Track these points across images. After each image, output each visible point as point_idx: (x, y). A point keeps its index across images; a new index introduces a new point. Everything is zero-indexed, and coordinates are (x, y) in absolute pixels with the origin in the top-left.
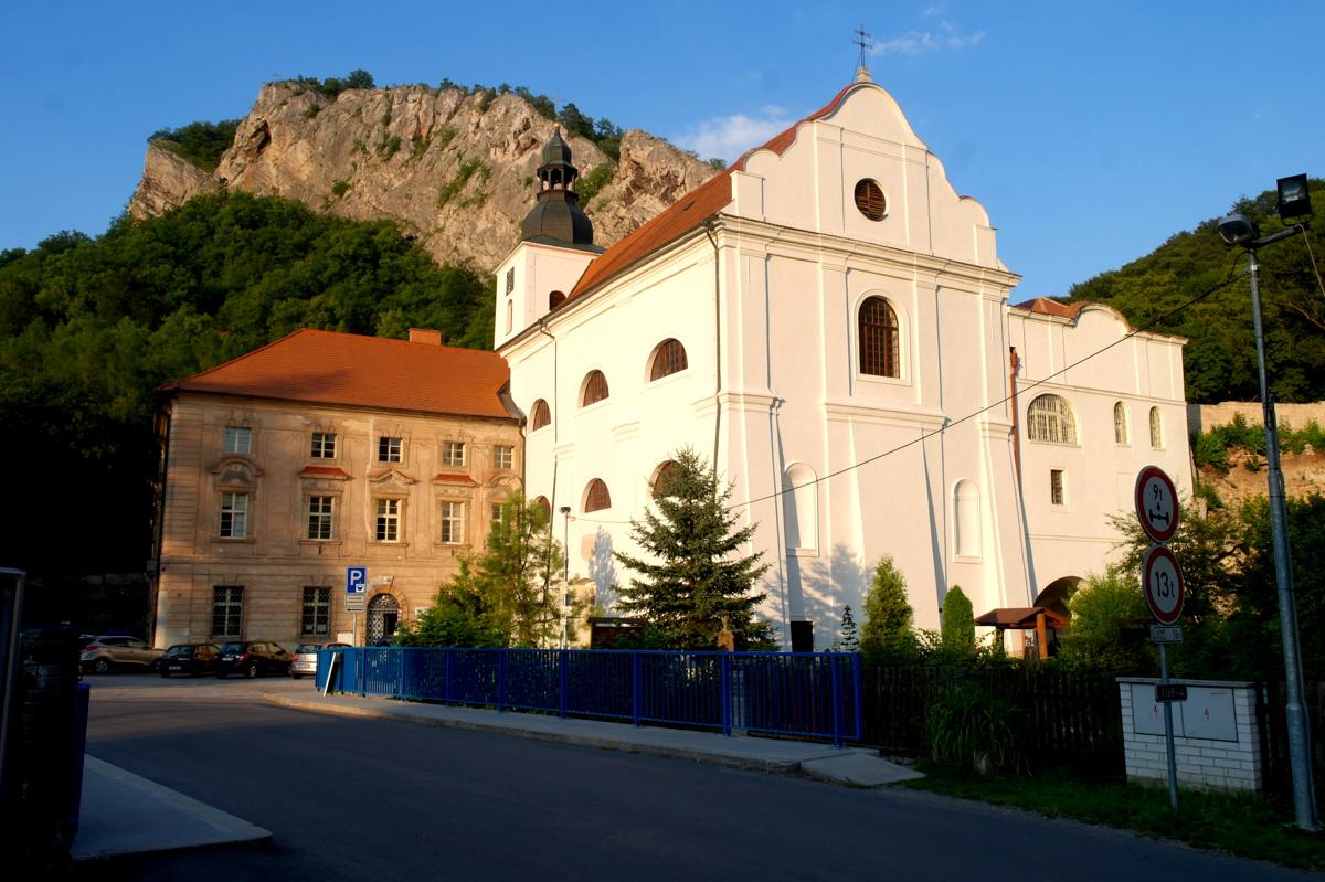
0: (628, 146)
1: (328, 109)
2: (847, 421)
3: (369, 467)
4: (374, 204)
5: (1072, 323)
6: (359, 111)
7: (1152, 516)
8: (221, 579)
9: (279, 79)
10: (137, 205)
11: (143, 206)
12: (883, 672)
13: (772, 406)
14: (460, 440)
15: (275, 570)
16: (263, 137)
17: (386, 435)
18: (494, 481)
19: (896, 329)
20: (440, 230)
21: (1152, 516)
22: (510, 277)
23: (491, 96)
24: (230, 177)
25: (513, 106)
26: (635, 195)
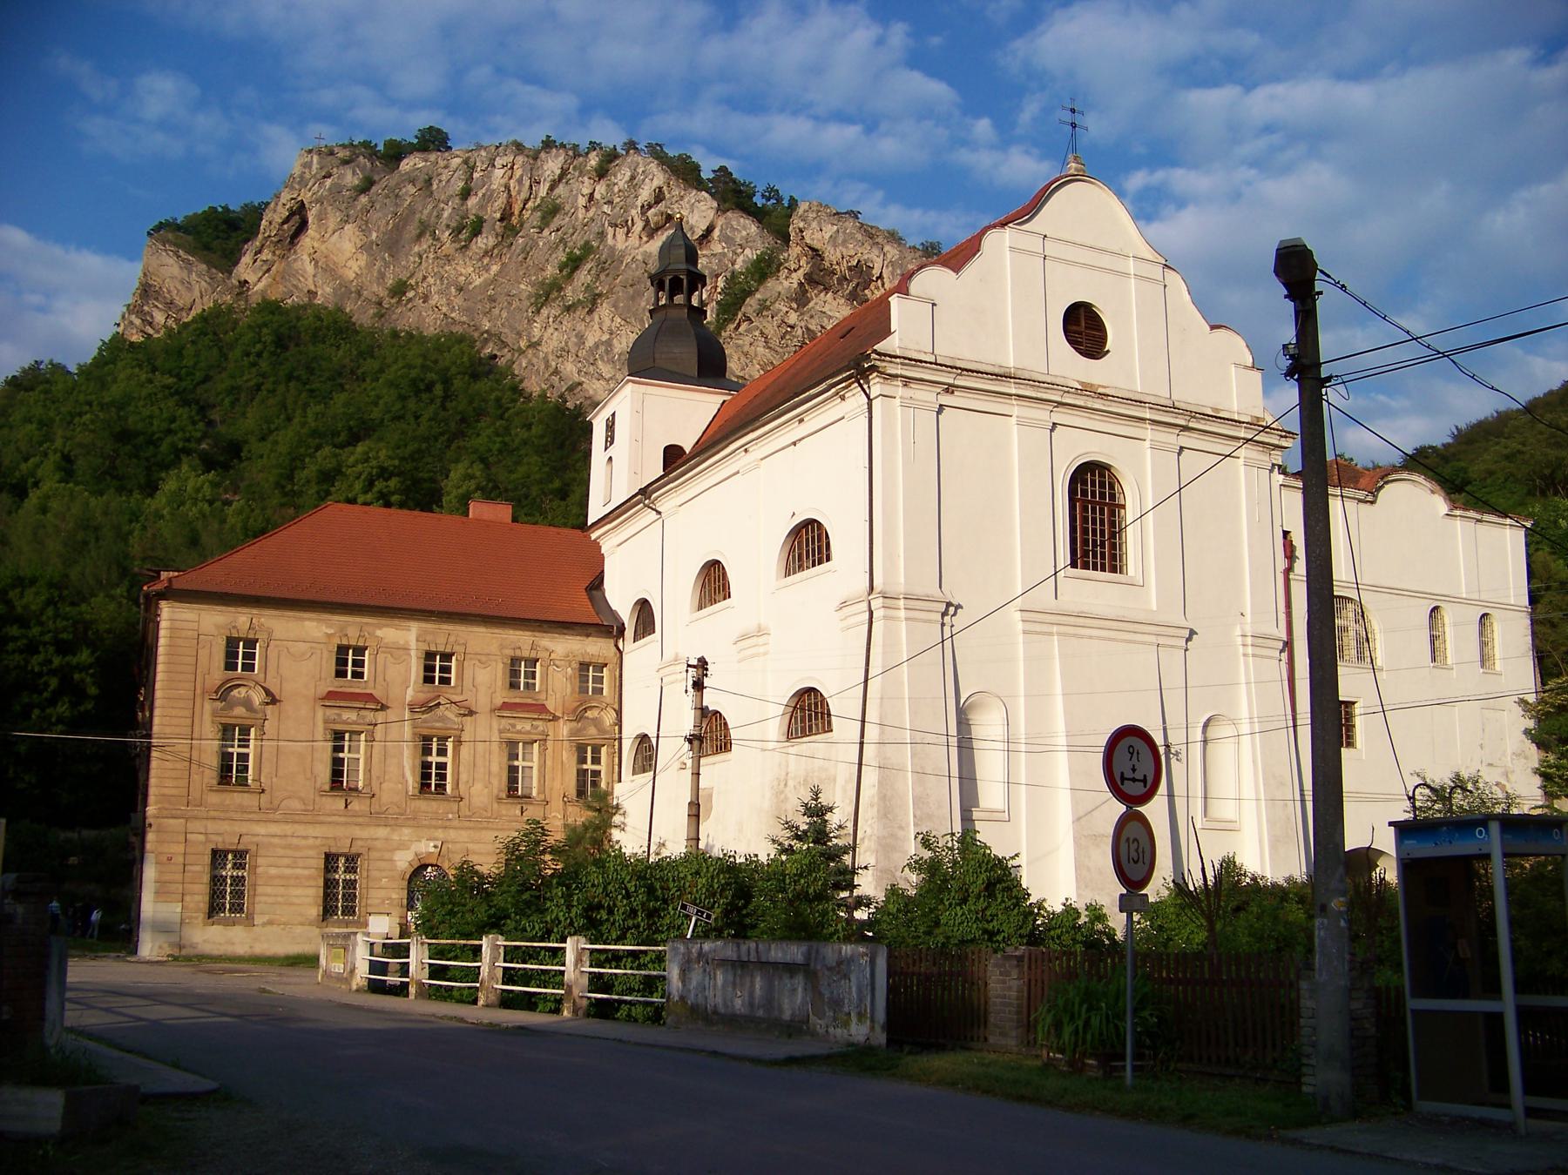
0: (801, 225)
1: (386, 181)
2: (1051, 634)
3: (410, 692)
4: (444, 309)
5: (1370, 498)
6: (429, 182)
7: (1123, 779)
8: (220, 839)
9: (323, 143)
10: (131, 323)
11: (138, 322)
13: (944, 614)
14: (533, 655)
15: (288, 829)
16: (298, 221)
18: (579, 715)
19: (1123, 507)
20: (534, 345)
21: (1123, 779)
22: (610, 426)
23: (611, 157)
24: (251, 278)
25: (640, 170)
26: (812, 293)
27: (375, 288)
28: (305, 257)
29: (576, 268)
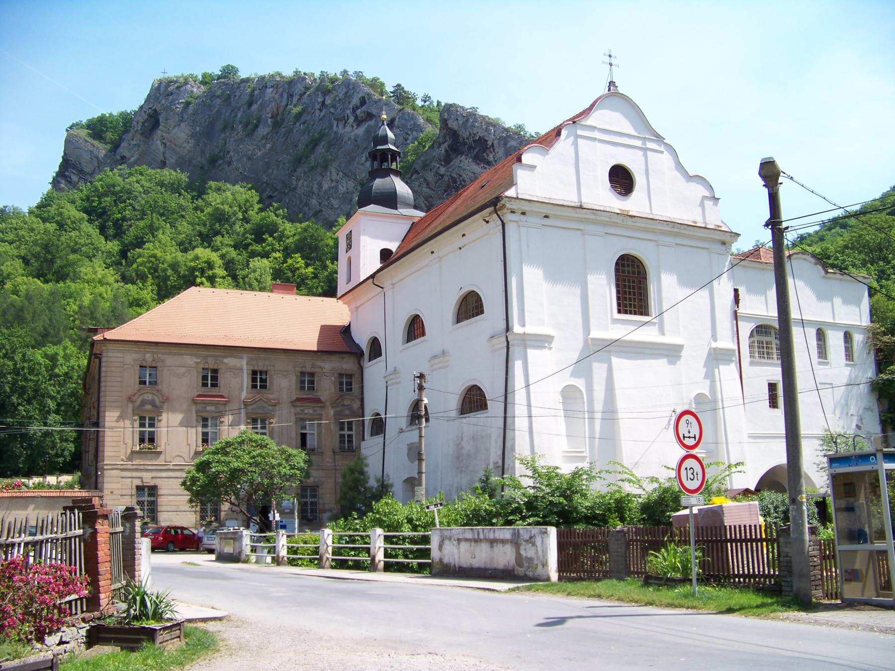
12: (718, 571)
17: (256, 368)
27: (199, 159)
28: (159, 142)
29: (316, 145)
